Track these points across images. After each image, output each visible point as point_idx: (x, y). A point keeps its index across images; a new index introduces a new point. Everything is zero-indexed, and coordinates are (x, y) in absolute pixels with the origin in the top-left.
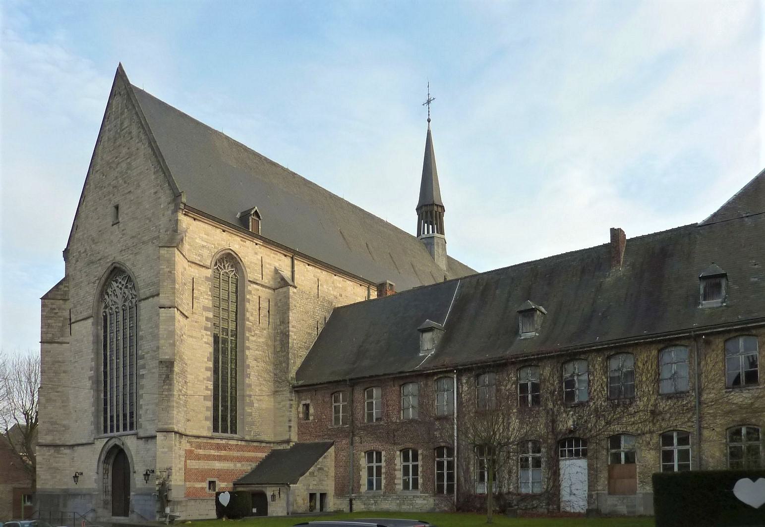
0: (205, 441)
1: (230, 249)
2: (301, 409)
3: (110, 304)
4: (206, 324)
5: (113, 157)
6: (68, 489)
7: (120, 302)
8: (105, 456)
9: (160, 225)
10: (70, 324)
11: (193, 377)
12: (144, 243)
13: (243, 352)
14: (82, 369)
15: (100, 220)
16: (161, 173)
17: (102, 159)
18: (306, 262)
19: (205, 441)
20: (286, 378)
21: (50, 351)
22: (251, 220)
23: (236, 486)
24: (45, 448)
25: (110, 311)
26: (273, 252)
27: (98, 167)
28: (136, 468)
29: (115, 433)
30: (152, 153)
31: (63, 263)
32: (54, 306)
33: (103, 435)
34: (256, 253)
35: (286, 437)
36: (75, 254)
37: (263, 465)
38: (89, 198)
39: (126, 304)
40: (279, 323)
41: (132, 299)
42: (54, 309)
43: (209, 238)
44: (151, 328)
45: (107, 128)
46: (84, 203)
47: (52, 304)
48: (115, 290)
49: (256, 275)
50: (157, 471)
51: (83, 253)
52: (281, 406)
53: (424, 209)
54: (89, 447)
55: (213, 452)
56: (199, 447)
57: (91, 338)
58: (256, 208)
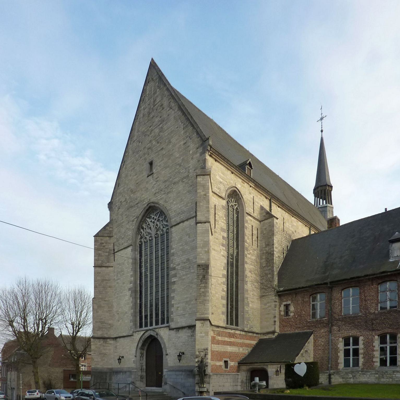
0: (222, 330)
1: (236, 187)
2: (282, 308)
3: (145, 235)
4: (223, 241)
5: (148, 127)
6: (112, 368)
7: (153, 232)
8: (141, 344)
9: (189, 167)
10: (114, 253)
12: (174, 183)
13: (243, 265)
14: (124, 283)
15: (137, 176)
16: (190, 127)
17: (138, 131)
18: (278, 204)
19: (222, 330)
20: (271, 285)
21: (100, 273)
22: (246, 168)
23: (240, 365)
24: (97, 340)
25: (145, 240)
26: (260, 194)
27: (135, 138)
28: (168, 351)
29: (149, 328)
30: (182, 114)
31: (108, 212)
32: (103, 241)
33: (139, 329)
34: (250, 193)
35: (271, 329)
36: (117, 204)
37: (256, 349)
38: (128, 162)
39: (158, 232)
40: (264, 246)
41: (163, 228)
42: (103, 243)
44: (182, 245)
45: (142, 108)
46: (124, 166)
47: (102, 240)
48: (149, 224)
49: (250, 209)
50: (197, 351)
51: (124, 201)
52: (267, 307)
53: (319, 189)
54: (129, 338)
55: (227, 339)
56: (219, 334)
57: (131, 261)
58: (250, 159)
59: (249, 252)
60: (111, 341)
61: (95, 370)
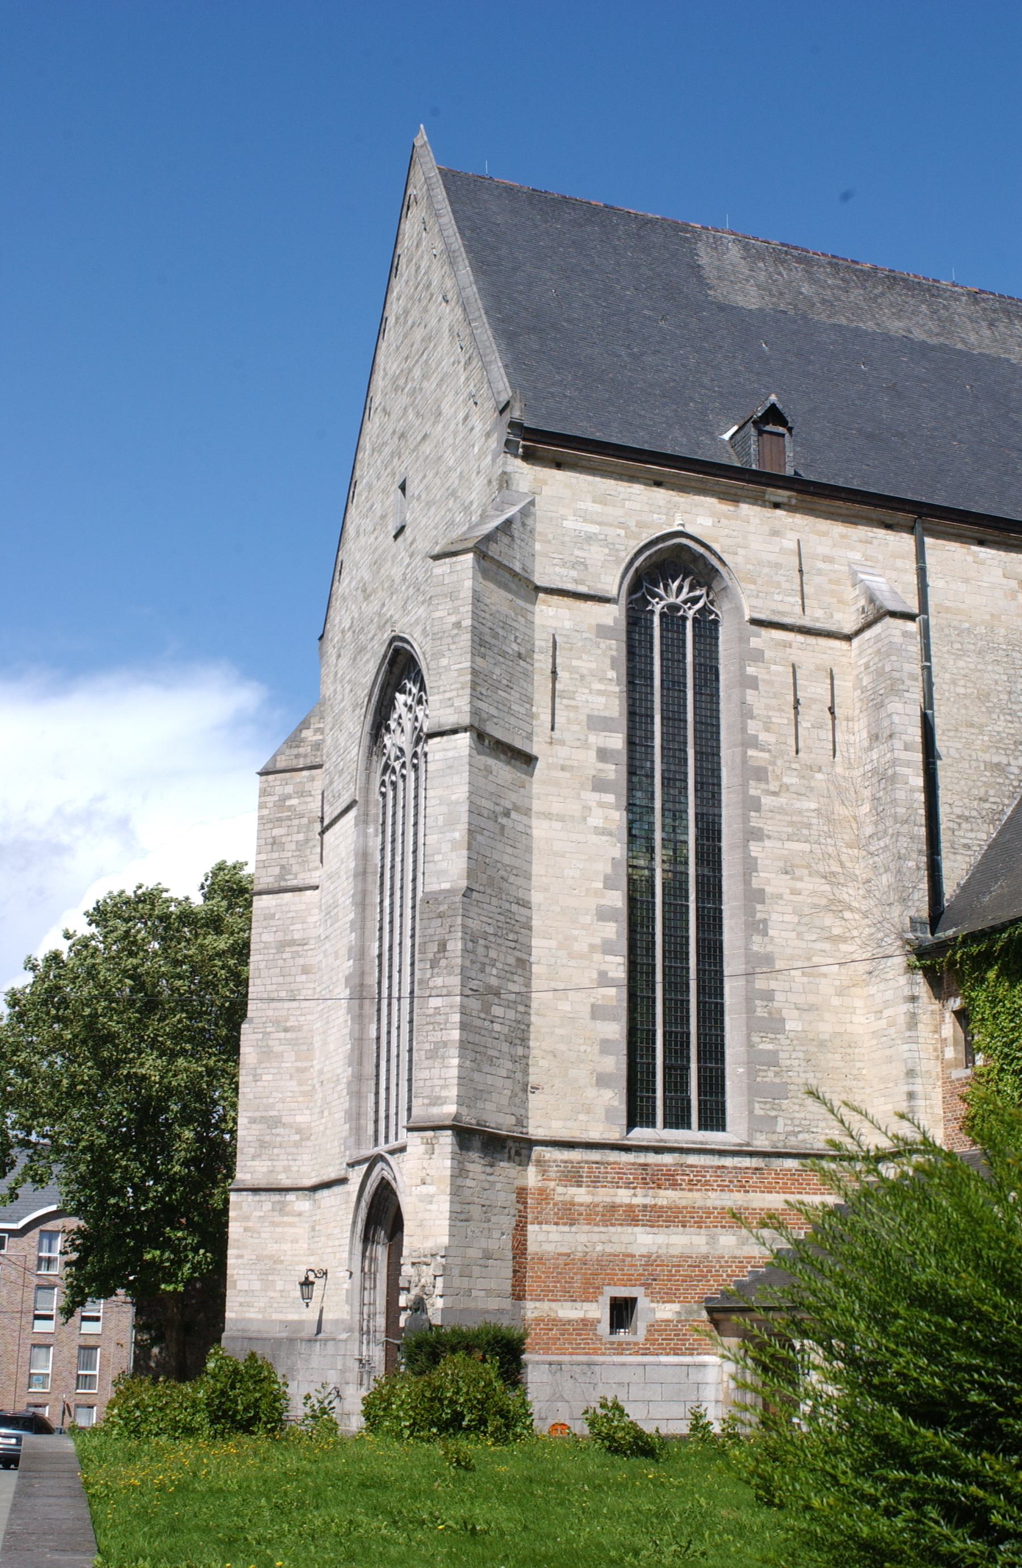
11: (553, 943)
34: (775, 533)
43: (609, 510)
55: (624, 1196)
59: (773, 786)
60: (301, 1203)
61: (239, 1330)
